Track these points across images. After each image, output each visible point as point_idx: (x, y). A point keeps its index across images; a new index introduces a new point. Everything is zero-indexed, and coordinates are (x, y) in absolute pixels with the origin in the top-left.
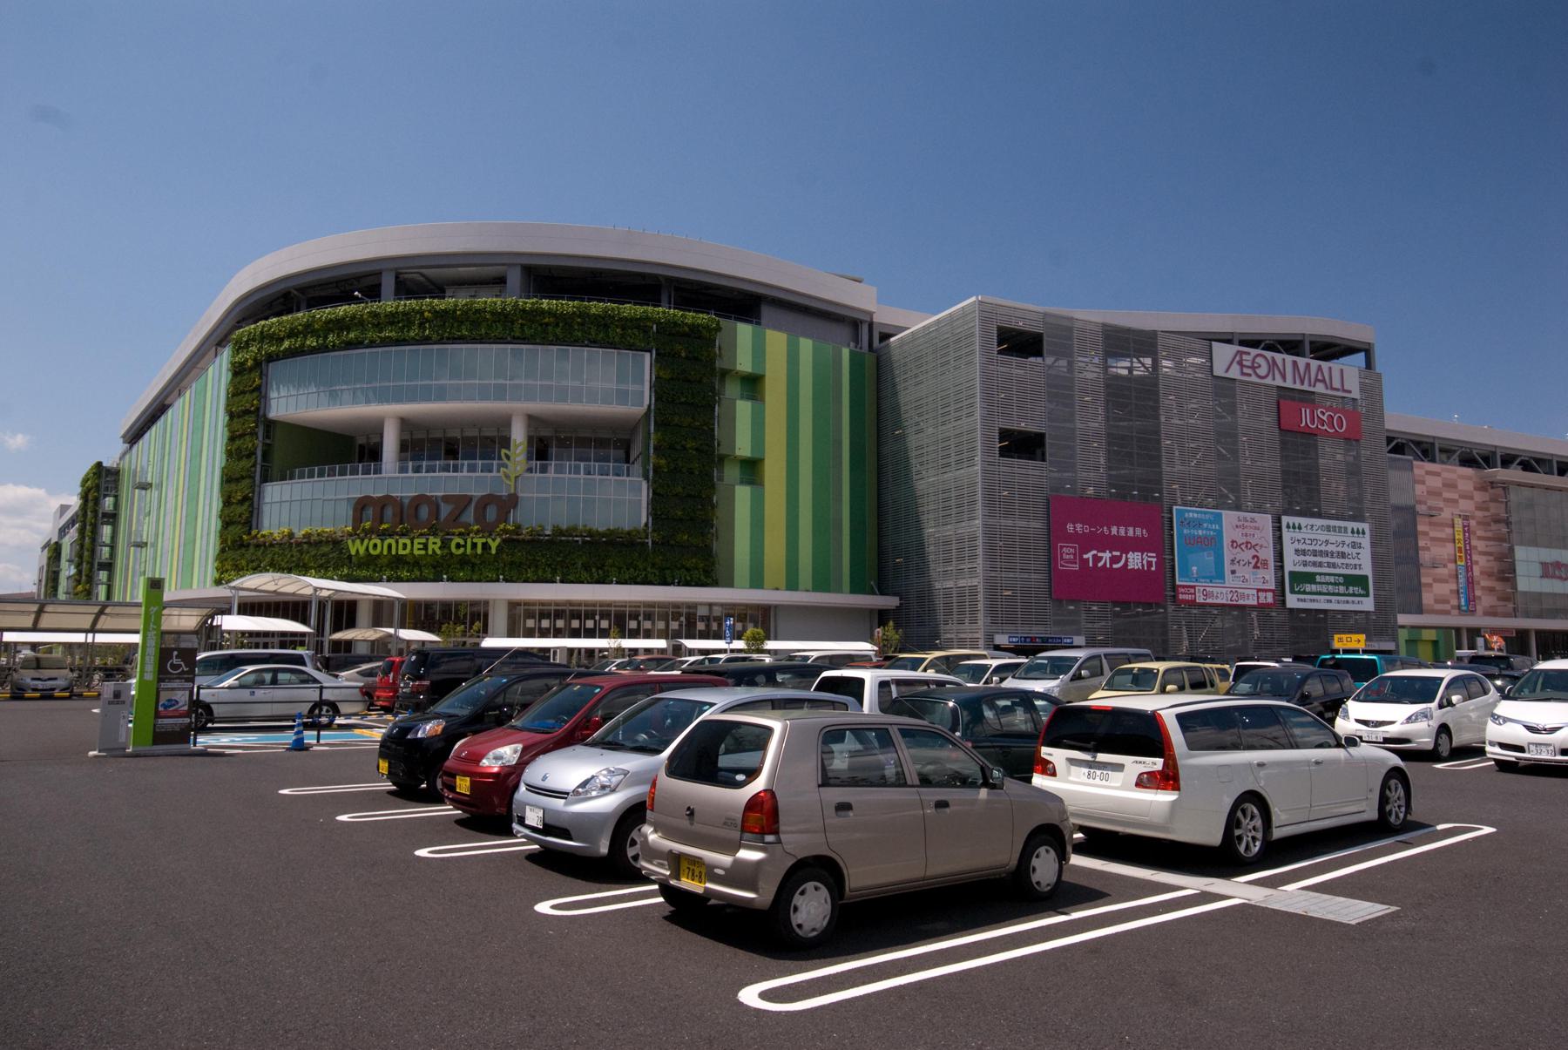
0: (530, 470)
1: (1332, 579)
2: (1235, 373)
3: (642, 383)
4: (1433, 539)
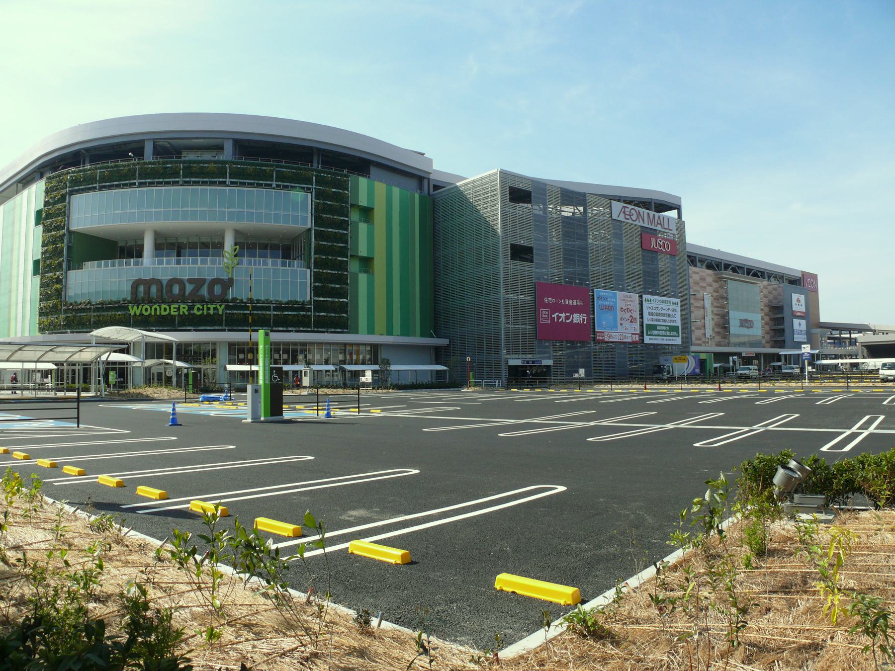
1: (663, 328)
2: (622, 218)
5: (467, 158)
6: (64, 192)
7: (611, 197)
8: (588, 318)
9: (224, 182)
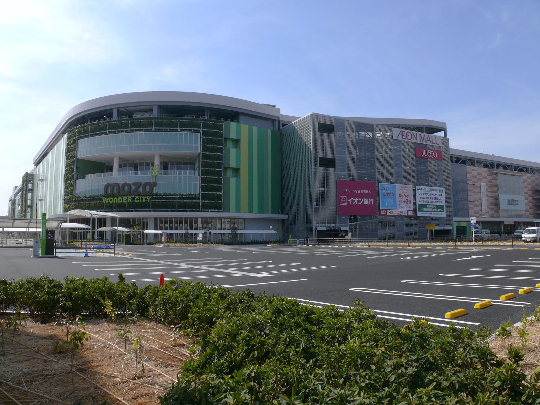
0: (161, 174)
1: (432, 206)
2: (400, 138)
3: (198, 143)
4: (474, 192)
5: (296, 107)
6: (74, 138)
7: (391, 125)
8: (375, 202)
9: (152, 129)
